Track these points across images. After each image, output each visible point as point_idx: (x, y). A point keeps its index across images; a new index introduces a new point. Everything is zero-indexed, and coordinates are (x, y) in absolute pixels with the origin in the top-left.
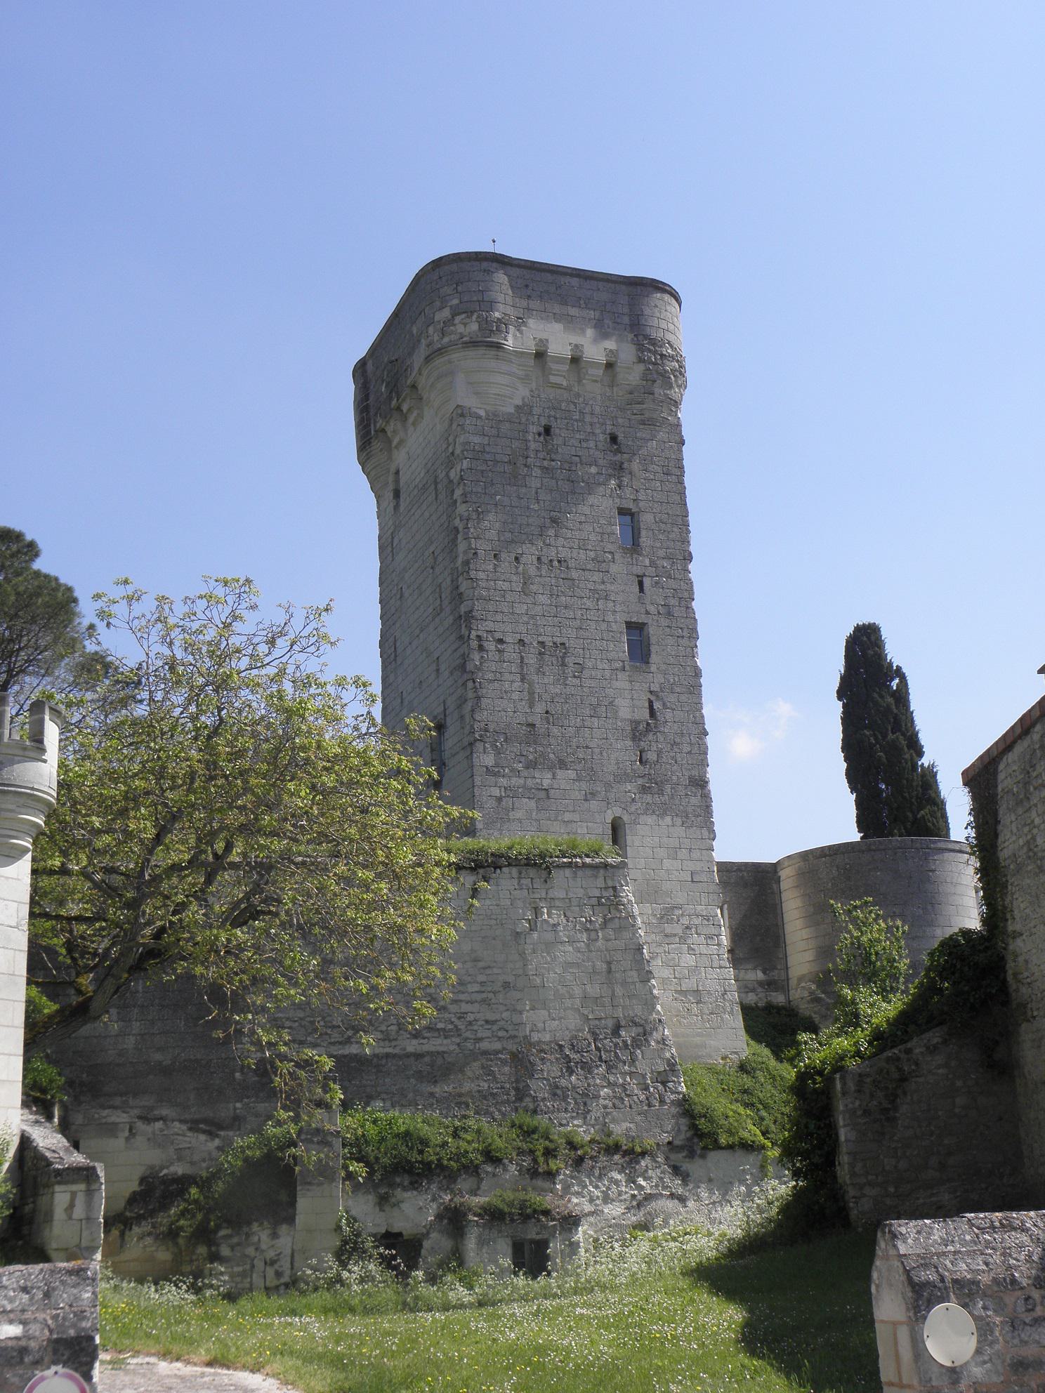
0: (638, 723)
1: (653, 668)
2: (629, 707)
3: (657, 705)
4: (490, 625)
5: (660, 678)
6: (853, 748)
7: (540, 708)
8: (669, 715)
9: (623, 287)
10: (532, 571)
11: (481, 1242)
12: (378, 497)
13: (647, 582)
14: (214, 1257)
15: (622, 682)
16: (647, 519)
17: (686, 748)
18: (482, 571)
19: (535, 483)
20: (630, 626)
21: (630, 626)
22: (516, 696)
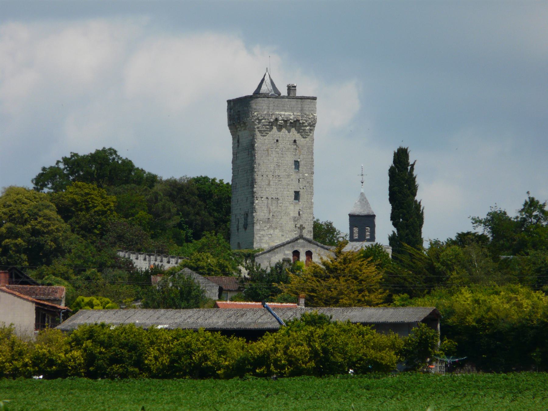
0: (295, 217)
1: (300, 203)
2: (293, 213)
3: (301, 213)
4: (260, 194)
5: (302, 206)
6: (392, 173)
7: (271, 214)
8: (304, 215)
9: (300, 100)
10: (271, 179)
11: (394, 232)
12: (233, 140)
13: (300, 180)
14: (460, 372)
15: (292, 207)
16: (302, 163)
17: (307, 224)
18: (272, 88)
19: (274, 156)
20: (295, 192)
21: (295, 192)
22: (265, 212)
